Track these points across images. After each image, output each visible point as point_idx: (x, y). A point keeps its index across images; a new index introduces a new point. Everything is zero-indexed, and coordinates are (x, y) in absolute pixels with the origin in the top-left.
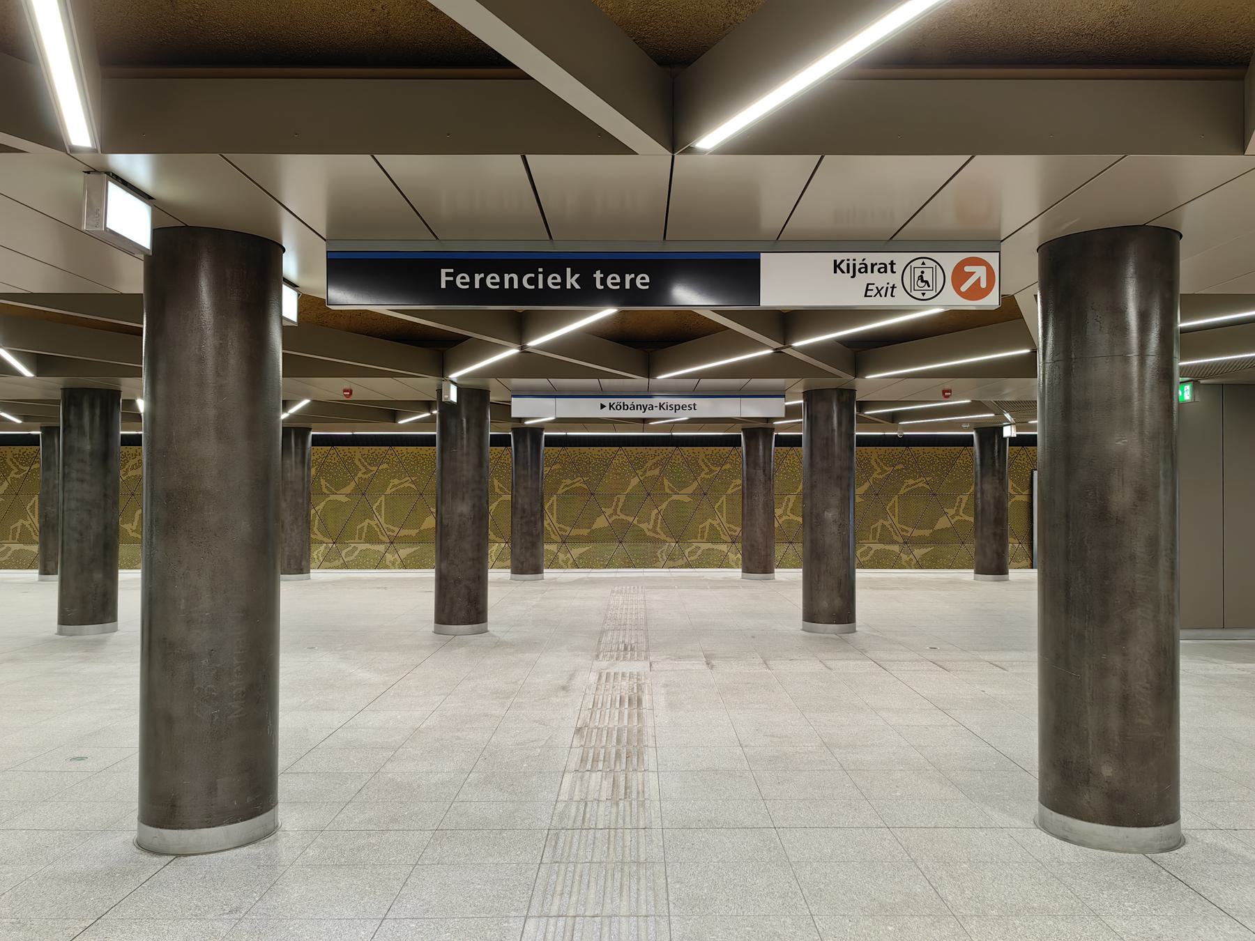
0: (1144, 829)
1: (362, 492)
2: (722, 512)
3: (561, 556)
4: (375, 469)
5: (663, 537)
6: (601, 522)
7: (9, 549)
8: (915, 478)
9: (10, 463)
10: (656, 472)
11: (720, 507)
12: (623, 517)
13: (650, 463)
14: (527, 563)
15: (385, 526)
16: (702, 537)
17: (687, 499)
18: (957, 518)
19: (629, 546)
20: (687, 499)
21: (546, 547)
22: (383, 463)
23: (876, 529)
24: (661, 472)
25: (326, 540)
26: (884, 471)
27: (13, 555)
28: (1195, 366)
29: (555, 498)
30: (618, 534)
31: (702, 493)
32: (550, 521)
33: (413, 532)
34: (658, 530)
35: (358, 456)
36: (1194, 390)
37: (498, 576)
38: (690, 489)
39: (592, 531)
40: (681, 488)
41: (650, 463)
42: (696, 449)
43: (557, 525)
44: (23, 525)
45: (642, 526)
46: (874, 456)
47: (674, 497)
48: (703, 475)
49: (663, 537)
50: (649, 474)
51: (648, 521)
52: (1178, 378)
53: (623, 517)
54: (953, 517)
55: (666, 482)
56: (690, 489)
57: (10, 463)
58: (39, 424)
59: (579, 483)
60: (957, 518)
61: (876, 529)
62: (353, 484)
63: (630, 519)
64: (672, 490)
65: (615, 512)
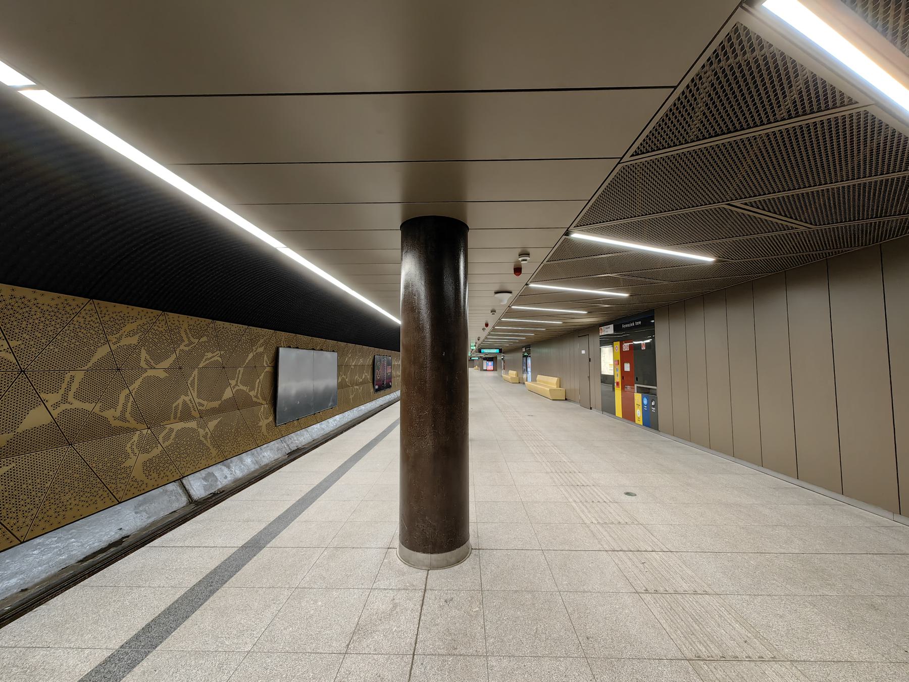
0: (141, 624)
2: (193, 387)
5: (133, 423)
7: (171, 430)
9: (183, 334)
10: (134, 340)
15: (197, 400)
20: (162, 374)
22: (204, 335)
23: (177, 407)
24: (140, 340)
25: (139, 426)
26: (191, 343)
27: (177, 436)
28: (89, 97)
29: (196, 372)
31: (178, 369)
34: (128, 415)
35: (185, 326)
36: (624, 357)
38: (166, 364)
41: (129, 327)
42: (20, 291)
43: (197, 400)
47: (150, 373)
50: (125, 341)
53: (77, 404)
54: (56, 405)
56: (166, 364)
57: (183, 334)
61: (199, 403)
65: (65, 399)
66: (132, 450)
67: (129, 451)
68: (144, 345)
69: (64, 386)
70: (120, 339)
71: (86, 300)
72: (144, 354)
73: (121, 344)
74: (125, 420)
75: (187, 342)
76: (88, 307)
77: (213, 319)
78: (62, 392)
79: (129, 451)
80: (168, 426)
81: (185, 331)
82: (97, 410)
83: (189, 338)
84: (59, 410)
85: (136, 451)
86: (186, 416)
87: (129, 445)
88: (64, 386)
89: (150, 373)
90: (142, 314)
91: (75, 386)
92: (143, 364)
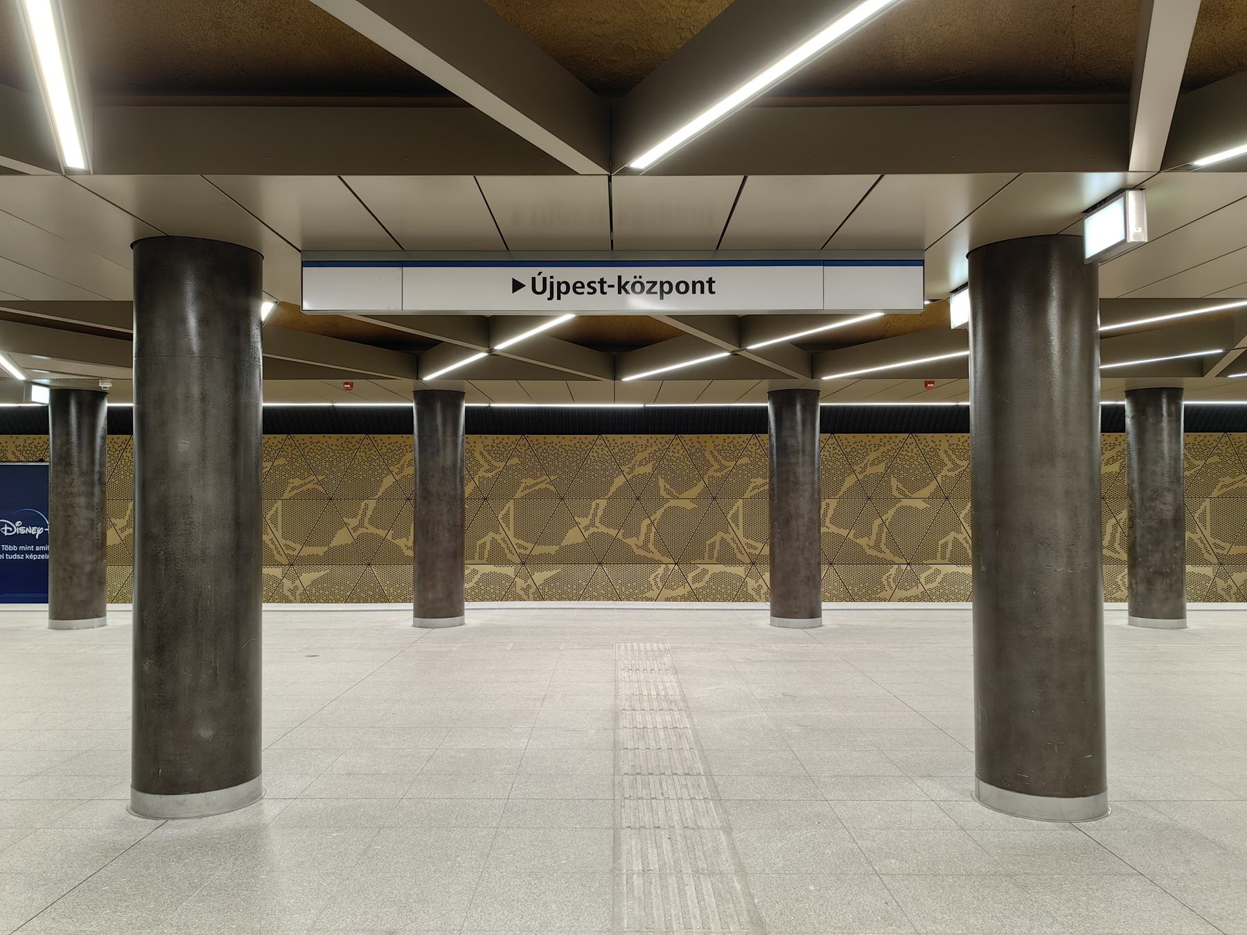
1: (712, 496)
3: (287, 584)
4: (1201, 463)
5: (657, 556)
6: (342, 538)
7: (705, 571)
8: (1233, 476)
9: (479, 457)
10: (648, 469)
11: (275, 517)
12: (372, 530)
13: (872, 456)
14: (1159, 596)
15: (744, 540)
16: (481, 558)
17: (690, 505)
18: (592, 530)
19: (599, 569)
21: (265, 570)
23: (946, 544)
25: (897, 560)
26: (957, 466)
30: (601, 553)
32: (273, 536)
33: (320, 551)
34: (651, 546)
35: (945, 446)
37: (1115, 615)
38: (694, 492)
39: (561, 548)
40: (913, 490)
41: (872, 456)
44: (723, 541)
45: (629, 541)
46: (945, 446)
47: (673, 503)
48: (711, 473)
49: (657, 556)
50: (869, 471)
51: (869, 535)
52: (77, 371)
53: (372, 530)
54: (586, 528)
55: (662, 483)
56: (694, 492)
57: (479, 457)
58: (765, 385)
59: (543, 483)
60: (592, 530)
62: (701, 485)
63: (382, 533)
64: (669, 493)
65: (361, 524)
66: (889, 583)
67: (652, 582)
68: (892, 472)
69: (361, 512)
70: (632, 469)
71: (284, 436)
72: (894, 482)
73: (636, 472)
74: (649, 551)
75: (716, 466)
76: (830, 441)
77: (289, 433)
78: (590, 517)
79: (885, 583)
80: (702, 567)
81: (481, 453)
82: (620, 536)
83: (488, 461)
84: (358, 533)
85: (893, 585)
86: (727, 557)
87: (652, 576)
88: (361, 512)
89: (906, 502)
90: (651, 441)
91: (830, 513)
92: (663, 493)
